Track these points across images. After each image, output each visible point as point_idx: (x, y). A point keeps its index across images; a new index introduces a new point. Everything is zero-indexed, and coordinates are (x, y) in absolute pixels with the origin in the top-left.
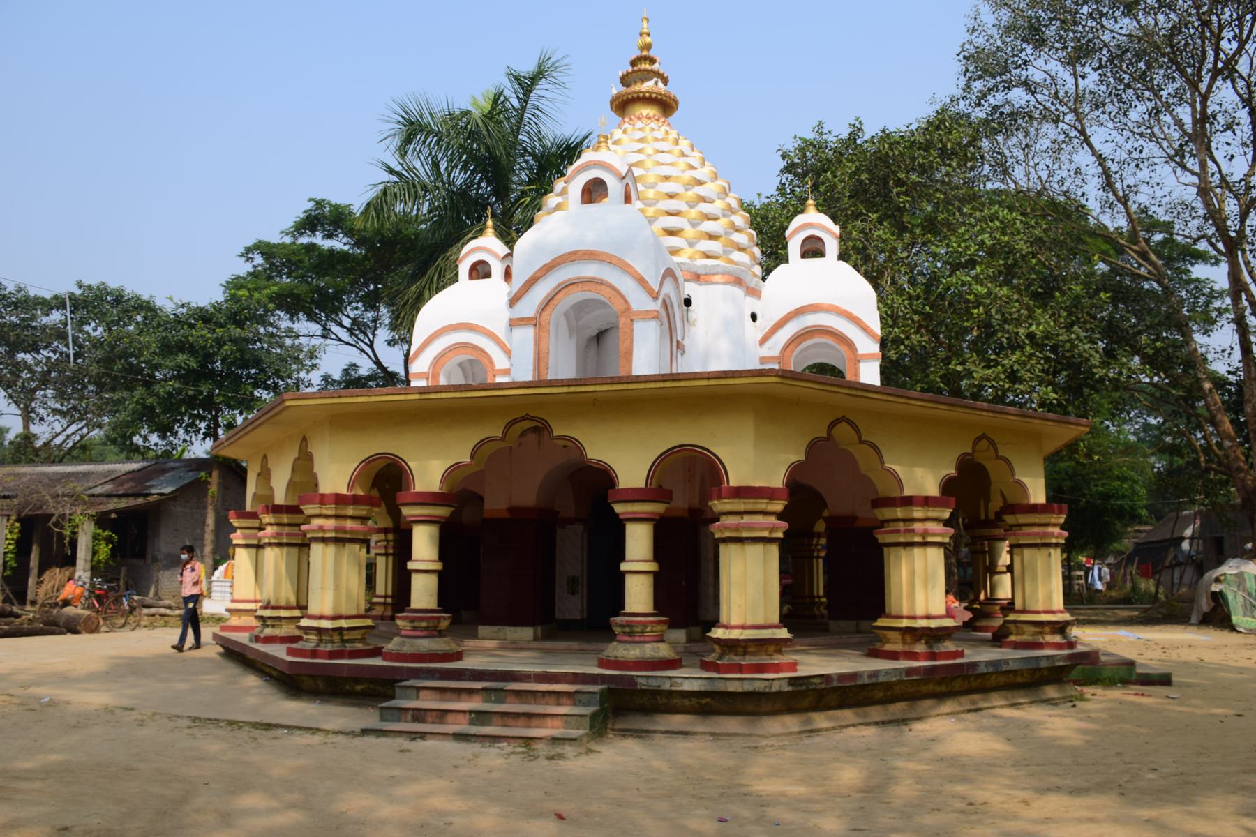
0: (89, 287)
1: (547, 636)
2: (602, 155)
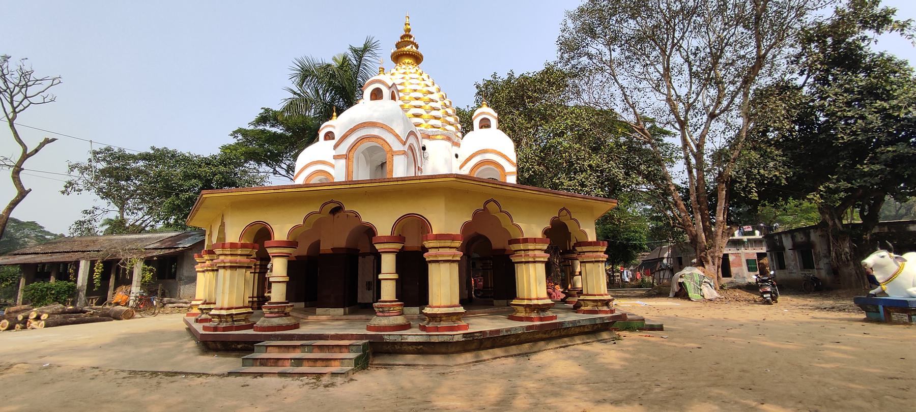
0: (158, 150)
1: (352, 313)
2: (381, 77)
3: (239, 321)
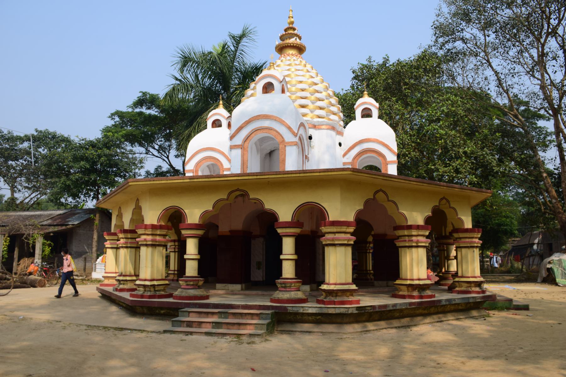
0: (41, 132)
1: (247, 288)
2: (272, 72)
3: (159, 291)
